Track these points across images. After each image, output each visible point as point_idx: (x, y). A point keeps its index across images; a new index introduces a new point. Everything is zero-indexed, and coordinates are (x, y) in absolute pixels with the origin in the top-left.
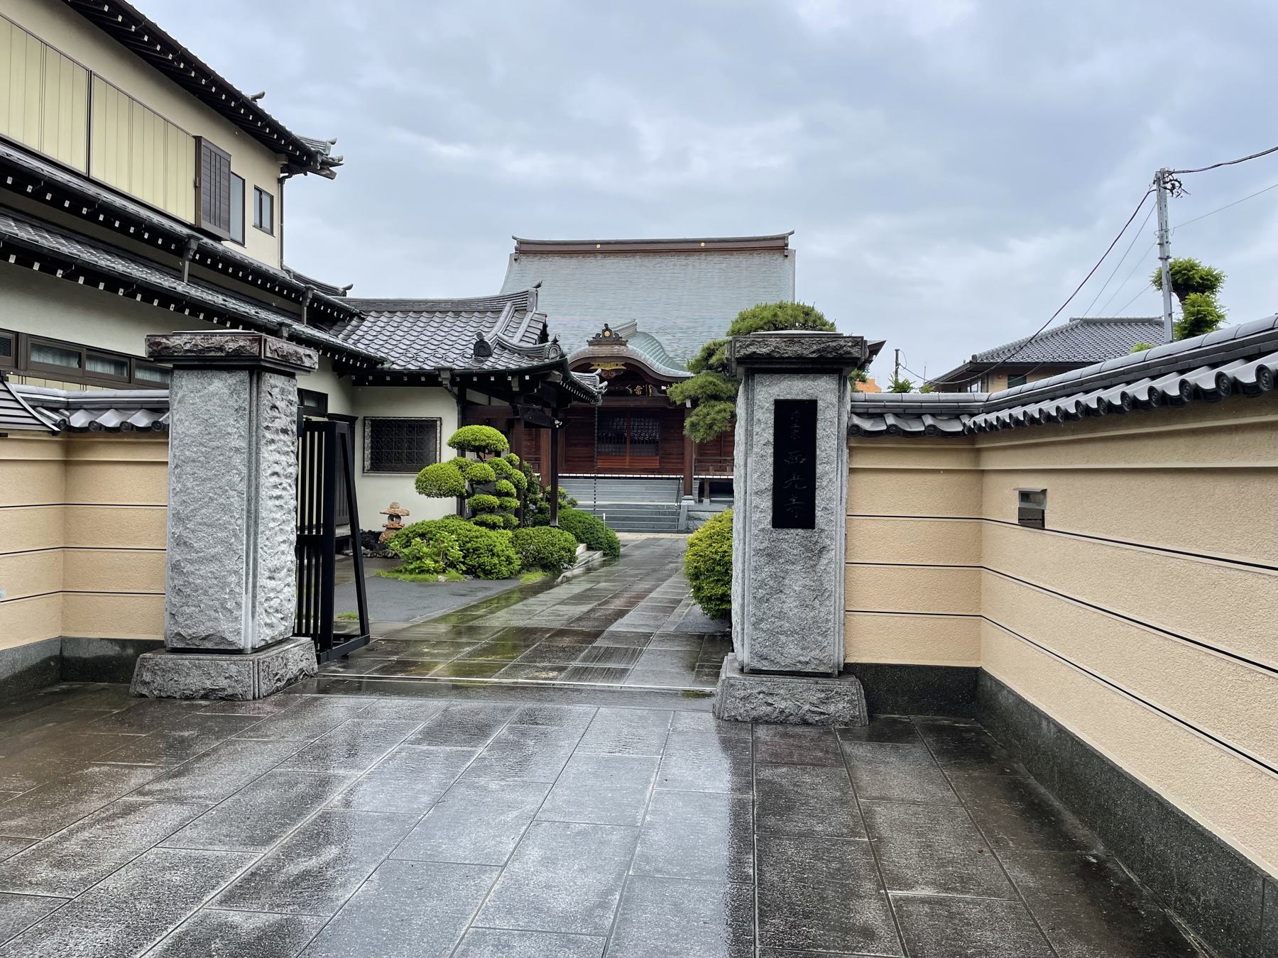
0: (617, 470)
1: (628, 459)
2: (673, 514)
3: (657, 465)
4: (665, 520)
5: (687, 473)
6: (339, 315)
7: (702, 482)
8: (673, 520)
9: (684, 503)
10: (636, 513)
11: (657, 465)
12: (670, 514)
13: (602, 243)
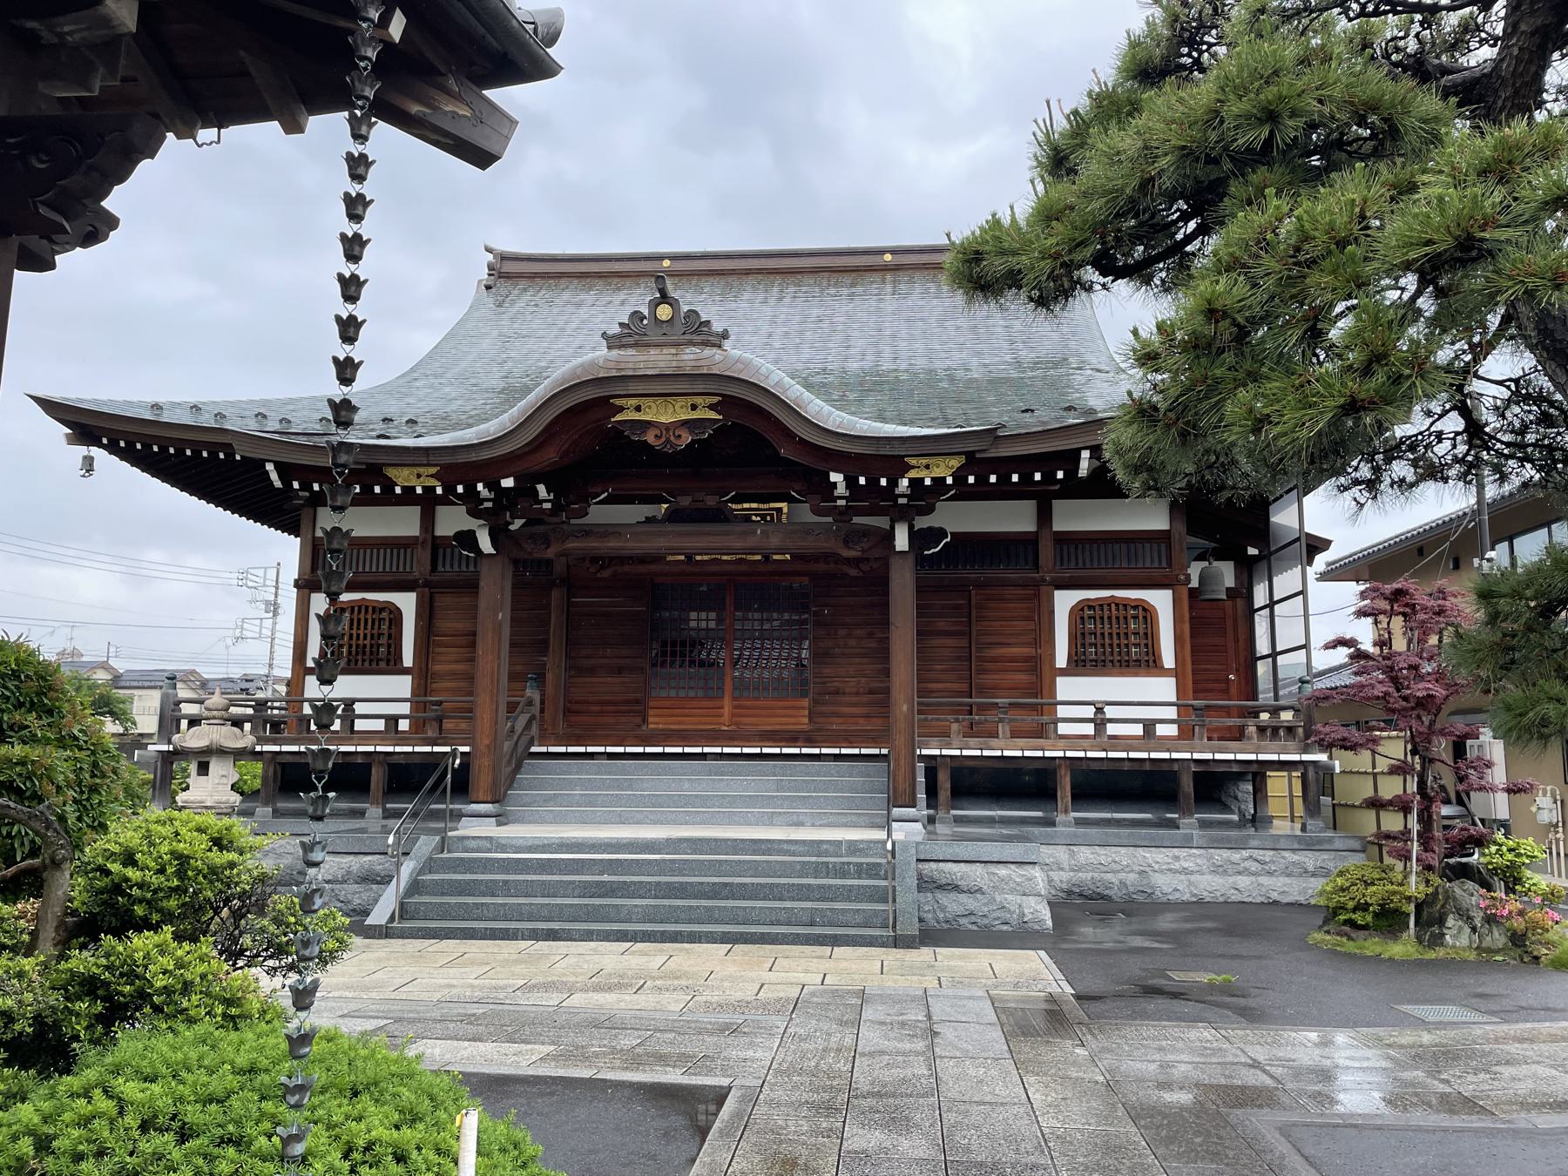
1: (727, 703)
2: (872, 871)
3: (802, 722)
4: (848, 894)
5: (900, 740)
7: (932, 765)
10: (755, 870)
11: (802, 722)
12: (860, 871)
13: (674, 257)
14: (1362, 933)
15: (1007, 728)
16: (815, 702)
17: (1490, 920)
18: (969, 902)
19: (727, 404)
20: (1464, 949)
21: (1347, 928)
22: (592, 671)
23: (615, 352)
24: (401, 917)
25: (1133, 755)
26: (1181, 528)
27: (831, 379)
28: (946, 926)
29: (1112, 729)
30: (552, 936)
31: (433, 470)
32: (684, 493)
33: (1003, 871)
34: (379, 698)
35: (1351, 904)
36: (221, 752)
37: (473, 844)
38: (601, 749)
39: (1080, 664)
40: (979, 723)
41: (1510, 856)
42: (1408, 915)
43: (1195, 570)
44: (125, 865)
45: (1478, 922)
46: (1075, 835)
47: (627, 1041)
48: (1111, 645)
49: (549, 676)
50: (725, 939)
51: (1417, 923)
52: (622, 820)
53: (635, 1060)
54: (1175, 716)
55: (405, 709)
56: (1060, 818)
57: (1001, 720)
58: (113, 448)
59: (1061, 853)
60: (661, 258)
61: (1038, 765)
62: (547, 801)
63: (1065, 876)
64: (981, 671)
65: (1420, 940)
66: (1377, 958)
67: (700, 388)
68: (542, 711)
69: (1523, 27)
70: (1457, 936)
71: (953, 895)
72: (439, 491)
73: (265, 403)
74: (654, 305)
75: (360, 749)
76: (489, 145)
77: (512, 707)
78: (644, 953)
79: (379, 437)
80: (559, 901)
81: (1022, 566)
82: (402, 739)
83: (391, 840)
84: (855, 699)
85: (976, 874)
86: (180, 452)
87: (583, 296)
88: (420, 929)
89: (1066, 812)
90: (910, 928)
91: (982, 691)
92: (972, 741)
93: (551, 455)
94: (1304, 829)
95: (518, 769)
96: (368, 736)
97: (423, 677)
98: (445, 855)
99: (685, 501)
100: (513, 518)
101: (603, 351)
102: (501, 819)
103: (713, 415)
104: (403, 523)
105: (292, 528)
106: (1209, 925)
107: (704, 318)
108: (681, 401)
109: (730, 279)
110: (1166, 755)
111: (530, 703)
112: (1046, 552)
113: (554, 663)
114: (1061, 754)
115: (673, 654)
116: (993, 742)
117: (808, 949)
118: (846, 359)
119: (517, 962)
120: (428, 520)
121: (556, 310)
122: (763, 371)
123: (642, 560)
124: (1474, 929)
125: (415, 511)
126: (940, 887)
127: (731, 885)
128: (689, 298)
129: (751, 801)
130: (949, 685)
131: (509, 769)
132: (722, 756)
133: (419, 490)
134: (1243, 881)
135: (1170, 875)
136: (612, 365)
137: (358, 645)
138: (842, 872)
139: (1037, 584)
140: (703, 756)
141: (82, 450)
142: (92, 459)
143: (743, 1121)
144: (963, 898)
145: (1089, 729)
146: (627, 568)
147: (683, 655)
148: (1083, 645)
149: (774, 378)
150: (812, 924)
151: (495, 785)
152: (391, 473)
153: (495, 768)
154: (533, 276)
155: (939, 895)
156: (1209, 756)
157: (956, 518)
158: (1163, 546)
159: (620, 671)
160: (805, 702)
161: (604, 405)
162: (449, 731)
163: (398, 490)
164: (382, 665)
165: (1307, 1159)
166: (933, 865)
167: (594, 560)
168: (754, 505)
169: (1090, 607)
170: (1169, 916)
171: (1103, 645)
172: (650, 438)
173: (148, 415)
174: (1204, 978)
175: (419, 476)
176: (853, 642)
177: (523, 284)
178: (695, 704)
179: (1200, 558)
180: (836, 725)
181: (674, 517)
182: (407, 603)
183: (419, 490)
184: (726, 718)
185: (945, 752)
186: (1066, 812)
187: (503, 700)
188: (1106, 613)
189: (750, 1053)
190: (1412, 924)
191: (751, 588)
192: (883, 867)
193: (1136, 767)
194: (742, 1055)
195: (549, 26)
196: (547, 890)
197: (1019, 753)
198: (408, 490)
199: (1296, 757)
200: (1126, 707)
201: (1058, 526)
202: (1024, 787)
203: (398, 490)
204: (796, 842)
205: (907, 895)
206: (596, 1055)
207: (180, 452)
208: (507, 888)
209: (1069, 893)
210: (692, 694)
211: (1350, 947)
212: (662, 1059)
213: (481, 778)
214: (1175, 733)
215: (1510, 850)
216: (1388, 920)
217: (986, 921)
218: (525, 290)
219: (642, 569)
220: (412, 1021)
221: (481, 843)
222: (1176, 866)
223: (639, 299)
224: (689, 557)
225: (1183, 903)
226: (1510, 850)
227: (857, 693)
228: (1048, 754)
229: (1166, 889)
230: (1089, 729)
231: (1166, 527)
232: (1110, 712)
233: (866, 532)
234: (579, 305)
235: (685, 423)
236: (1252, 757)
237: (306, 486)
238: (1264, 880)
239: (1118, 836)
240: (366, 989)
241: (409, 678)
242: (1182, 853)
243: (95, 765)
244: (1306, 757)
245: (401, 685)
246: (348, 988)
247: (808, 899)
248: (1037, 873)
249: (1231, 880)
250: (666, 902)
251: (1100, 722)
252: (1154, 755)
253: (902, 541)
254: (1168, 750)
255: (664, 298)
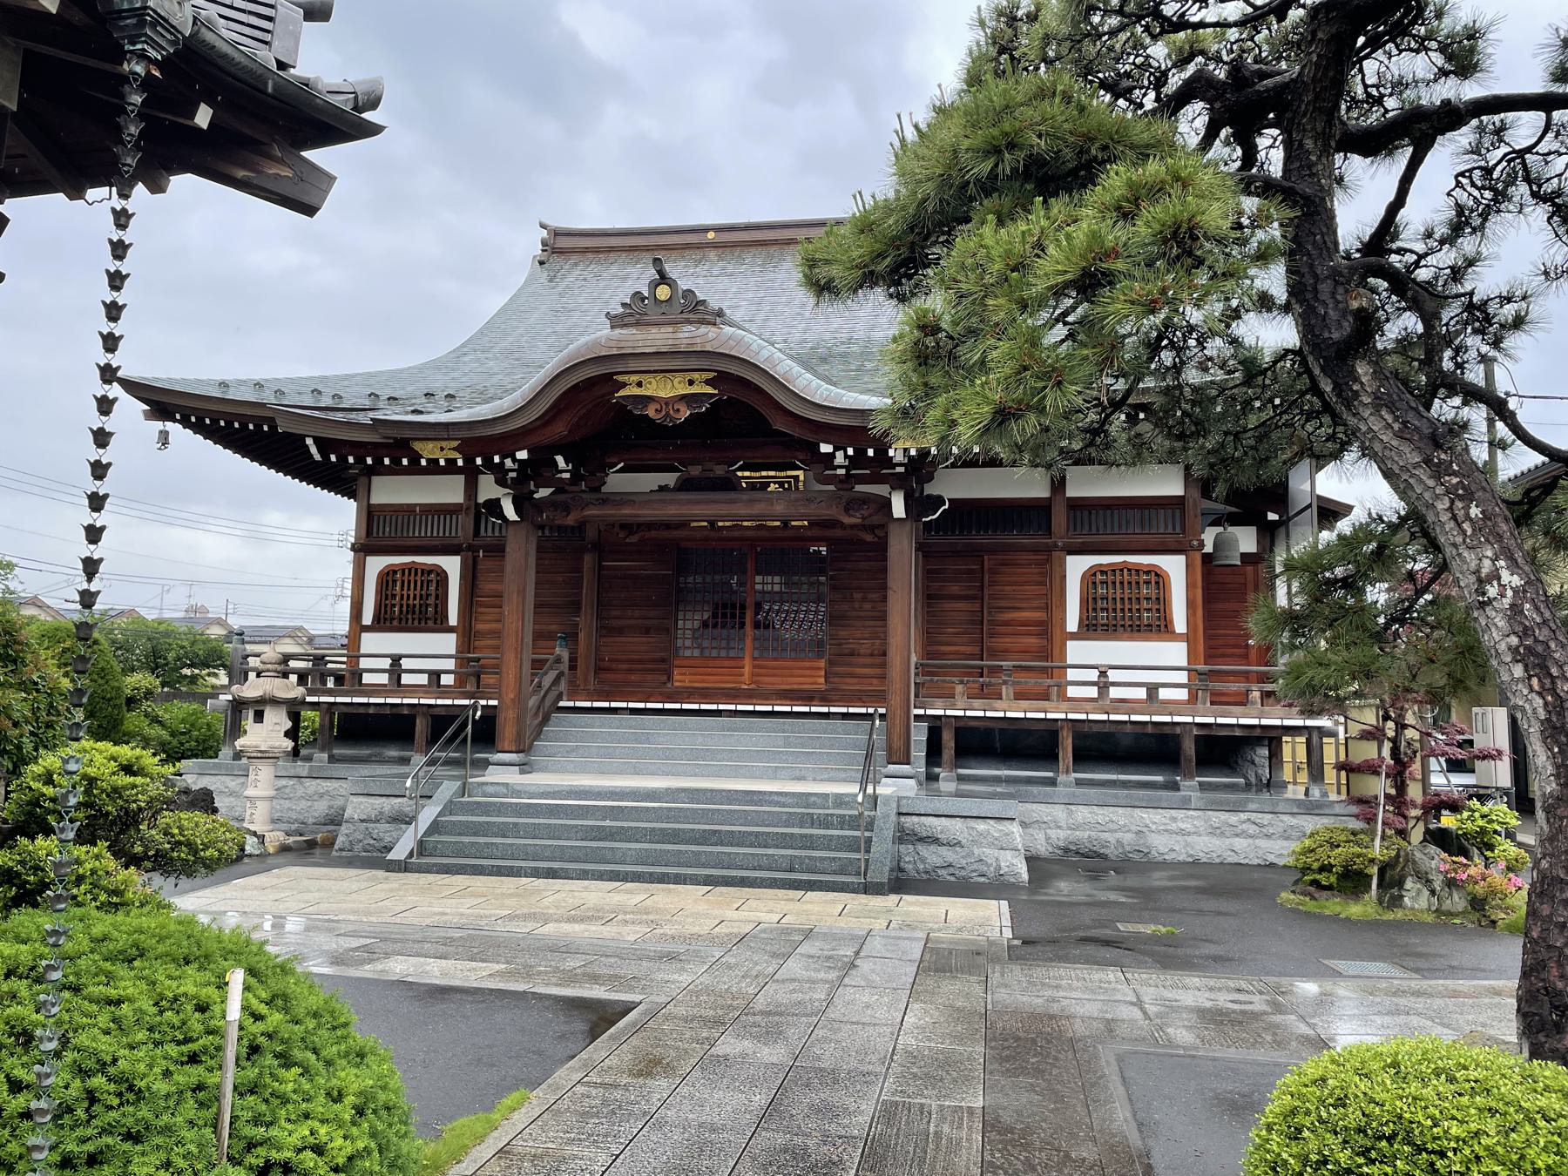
0: (714, 695)
1: (747, 663)
2: (853, 822)
4: (828, 843)
5: (896, 700)
6: (360, 460)
7: (935, 729)
8: (853, 845)
9: (886, 788)
10: (745, 818)
12: (844, 822)
13: (719, 229)
14: (1326, 893)
15: (1011, 691)
16: (831, 663)
17: (1451, 883)
18: (948, 855)
19: (720, 379)
20: (1422, 911)
21: (1312, 889)
22: (620, 631)
23: (618, 331)
24: (420, 854)
25: (1134, 718)
26: (1196, 493)
27: (855, 348)
28: (925, 876)
29: (1114, 693)
30: (552, 874)
31: (455, 444)
32: (694, 462)
33: (981, 826)
34: (429, 651)
35: (1316, 866)
36: (274, 702)
37: (491, 789)
38: (624, 705)
39: (1091, 628)
40: (989, 685)
41: (1481, 822)
42: (1371, 877)
43: (1209, 537)
44: (45, 783)
45: (1437, 885)
46: (1073, 795)
47: (572, 963)
48: (1123, 610)
49: (581, 636)
50: (709, 881)
51: (1379, 886)
52: (637, 772)
53: (571, 978)
54: (1185, 681)
55: (450, 664)
56: (1062, 778)
57: (1005, 682)
58: (185, 423)
59: (1059, 812)
60: (706, 230)
61: (1041, 727)
62: (570, 751)
63: (1062, 834)
64: (991, 635)
65: (1380, 902)
66: (1335, 918)
67: (693, 364)
68: (573, 667)
69: (1320, 35)
70: (1416, 898)
71: (933, 848)
72: (460, 463)
73: (323, 379)
74: (654, 285)
75: (406, 701)
76: (306, 199)
77: (538, 664)
78: (628, 892)
79: (415, 412)
80: (562, 843)
81: (1031, 530)
82: (445, 692)
83: (408, 784)
84: (868, 660)
85: (955, 828)
86: (244, 426)
87: (630, 269)
88: (435, 865)
89: (1067, 772)
90: (881, 875)
91: (995, 654)
92: (977, 703)
93: (560, 429)
94: (1307, 794)
95: (546, 720)
96: (414, 689)
97: (468, 635)
98: (466, 799)
99: (695, 471)
100: (538, 486)
101: (607, 331)
102: (525, 767)
103: (709, 390)
104: (449, 491)
105: (351, 495)
106: (1193, 883)
107: (701, 297)
108: (678, 378)
109: (772, 249)
110: (1167, 719)
111: (558, 660)
112: (1059, 518)
113: (586, 623)
114: (1062, 716)
115: (724, 616)
116: (998, 704)
117: (781, 893)
118: (873, 328)
119: (511, 895)
120: (471, 488)
121: (602, 284)
122: (754, 347)
123: (668, 526)
124: (1433, 892)
125: (460, 480)
126: (921, 840)
127: (719, 832)
128: (688, 276)
129: (760, 756)
130: (963, 648)
131: (537, 722)
132: (736, 713)
133: (442, 463)
134: (1240, 844)
135: (1167, 835)
136: (613, 344)
137: (407, 605)
138: (825, 823)
139: (1049, 550)
140: (718, 713)
141: (159, 425)
142: (167, 433)
143: (638, 1028)
144: (943, 851)
145: (1093, 692)
146: (654, 534)
147: (733, 616)
148: (1095, 610)
149: (765, 354)
150: (791, 870)
151: (519, 736)
152: (417, 446)
153: (520, 720)
154: (597, 250)
155: (920, 847)
156: (1211, 720)
157: (952, 486)
158: (1178, 512)
159: (647, 631)
160: (822, 663)
161: (608, 381)
162: (488, 686)
163: (423, 462)
164: (430, 623)
165: (1123, 1078)
166: (915, 819)
167: (623, 526)
168: (772, 473)
169: (1102, 572)
170: (1157, 875)
171: (1114, 610)
172: (651, 412)
173: (215, 393)
174: (1149, 929)
175: (442, 449)
176: (867, 606)
177: (574, 258)
178: (718, 663)
179: (1214, 523)
180: (852, 685)
181: (685, 486)
182: (452, 565)
183: (442, 463)
184: (746, 677)
185: (949, 713)
186: (1067, 772)
187: (528, 656)
188: (1118, 578)
189: (676, 976)
190: (1374, 886)
191: (778, 551)
192: (858, 823)
193: (1138, 729)
194: (666, 977)
195: (368, 94)
196: (552, 832)
197: (1021, 715)
198: (433, 462)
199: (1300, 723)
200: (1142, 673)
201: (1072, 492)
202: (1028, 747)
203: (423, 462)
204: (786, 794)
205: (883, 847)
206: (539, 973)
207: (244, 426)
208: (516, 830)
209: (1066, 850)
210: (714, 653)
211: (1311, 906)
212: (595, 979)
213: (507, 729)
214: (1186, 697)
215: (1483, 817)
216: (1352, 881)
217: (963, 873)
218: (576, 264)
219: (666, 534)
220: (396, 941)
221: (498, 788)
222: (1174, 827)
223: (639, 277)
224: (712, 523)
225: (1180, 863)
226: (1483, 817)
227: (872, 655)
228: (1050, 716)
229: (1162, 850)
230: (1093, 692)
231: (1180, 492)
232: (1113, 676)
233: (867, 499)
234: (624, 279)
235: (683, 397)
236: (1255, 722)
237: (360, 460)
238: (1263, 843)
239: (1116, 796)
240: (369, 914)
241: (454, 636)
242: (1180, 814)
243: (51, 706)
244: (1309, 723)
245: (446, 643)
246: (355, 912)
247: (791, 847)
248: (1015, 828)
249: (1228, 841)
250: (658, 846)
251: (1103, 685)
252: (1156, 719)
253: (898, 508)
254: (1171, 714)
255: (663, 279)
